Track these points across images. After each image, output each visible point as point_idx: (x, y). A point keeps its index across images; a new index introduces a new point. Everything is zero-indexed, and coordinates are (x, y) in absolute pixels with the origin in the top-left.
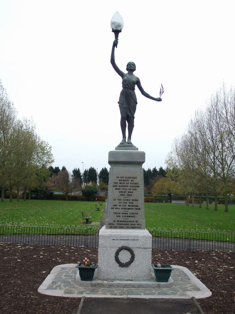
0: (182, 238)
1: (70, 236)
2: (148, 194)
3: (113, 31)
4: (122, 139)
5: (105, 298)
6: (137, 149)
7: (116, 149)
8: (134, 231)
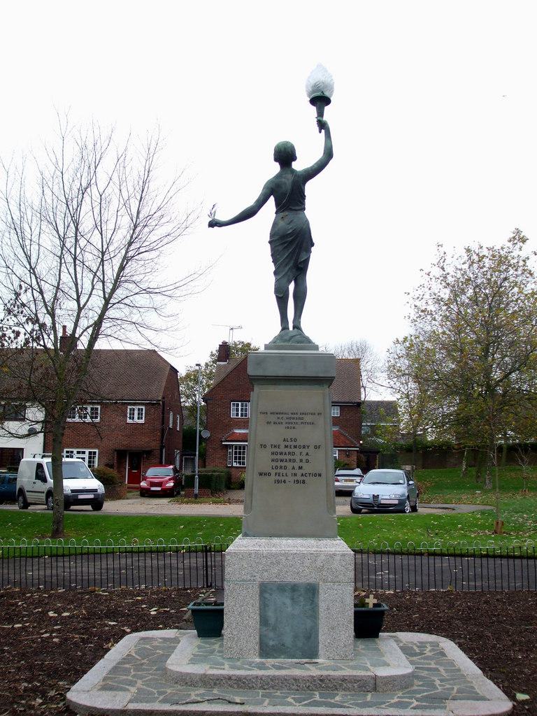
0: (101, 553)
1: (425, 559)
2: (502, 452)
3: (314, 101)
4: (279, 328)
5: (152, 712)
6: (316, 348)
7: (267, 347)
8: (313, 542)
